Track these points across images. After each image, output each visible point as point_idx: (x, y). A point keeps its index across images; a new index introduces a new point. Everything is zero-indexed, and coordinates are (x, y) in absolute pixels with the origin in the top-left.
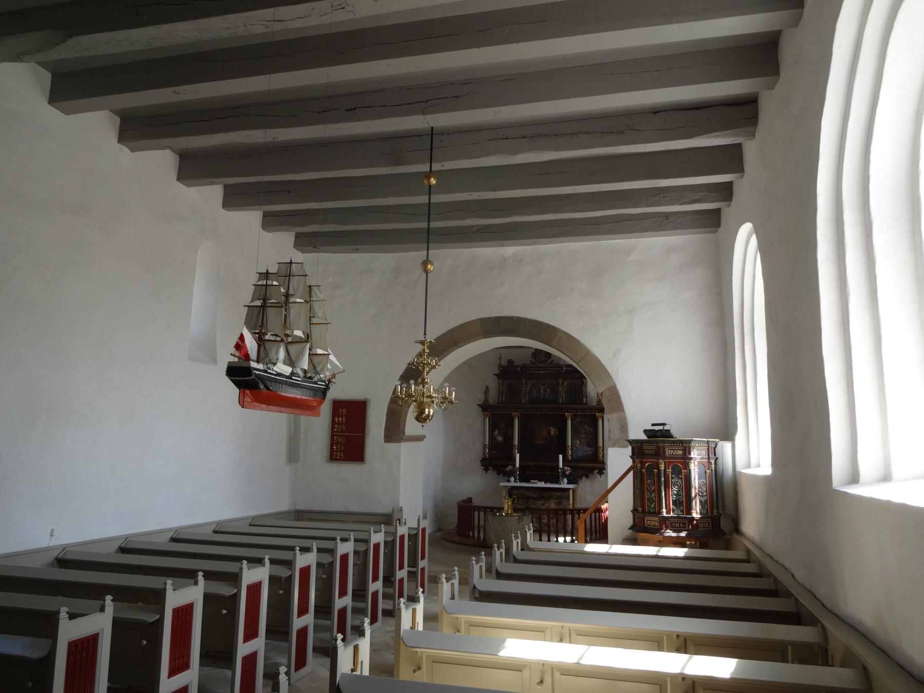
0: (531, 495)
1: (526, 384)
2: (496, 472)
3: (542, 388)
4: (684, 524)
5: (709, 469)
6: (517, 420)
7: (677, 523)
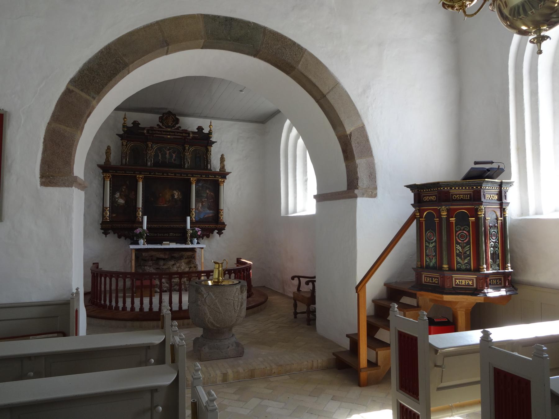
0: (162, 256)
1: (152, 147)
2: (116, 235)
3: (168, 152)
4: (500, 279)
5: (501, 217)
6: (141, 183)
7: (494, 279)
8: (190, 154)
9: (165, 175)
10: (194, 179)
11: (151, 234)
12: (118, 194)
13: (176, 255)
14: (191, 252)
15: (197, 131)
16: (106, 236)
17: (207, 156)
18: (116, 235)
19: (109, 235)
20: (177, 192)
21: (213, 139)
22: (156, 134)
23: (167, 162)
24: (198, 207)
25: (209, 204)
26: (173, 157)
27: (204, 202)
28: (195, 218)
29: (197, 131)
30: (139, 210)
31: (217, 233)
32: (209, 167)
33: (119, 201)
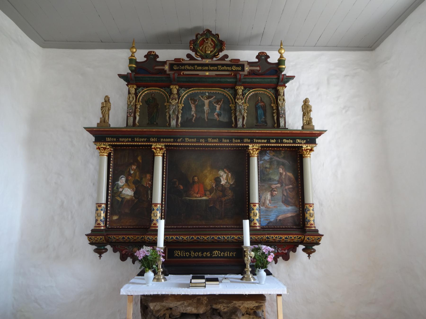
2: (118, 254)
3: (207, 102)
8: (245, 103)
9: (202, 142)
10: (255, 147)
11: (179, 253)
12: (123, 179)
13: (222, 308)
14: (254, 302)
15: (257, 60)
16: (100, 257)
17: (277, 104)
18: (118, 254)
19: (105, 254)
20: (225, 173)
21: (288, 72)
22: (185, 70)
23: (206, 119)
24: (265, 200)
25: (285, 194)
26: (216, 109)
27: (275, 189)
28: (260, 221)
29: (257, 60)
30: (155, 208)
31: (304, 250)
32: (282, 124)
33: (124, 192)
